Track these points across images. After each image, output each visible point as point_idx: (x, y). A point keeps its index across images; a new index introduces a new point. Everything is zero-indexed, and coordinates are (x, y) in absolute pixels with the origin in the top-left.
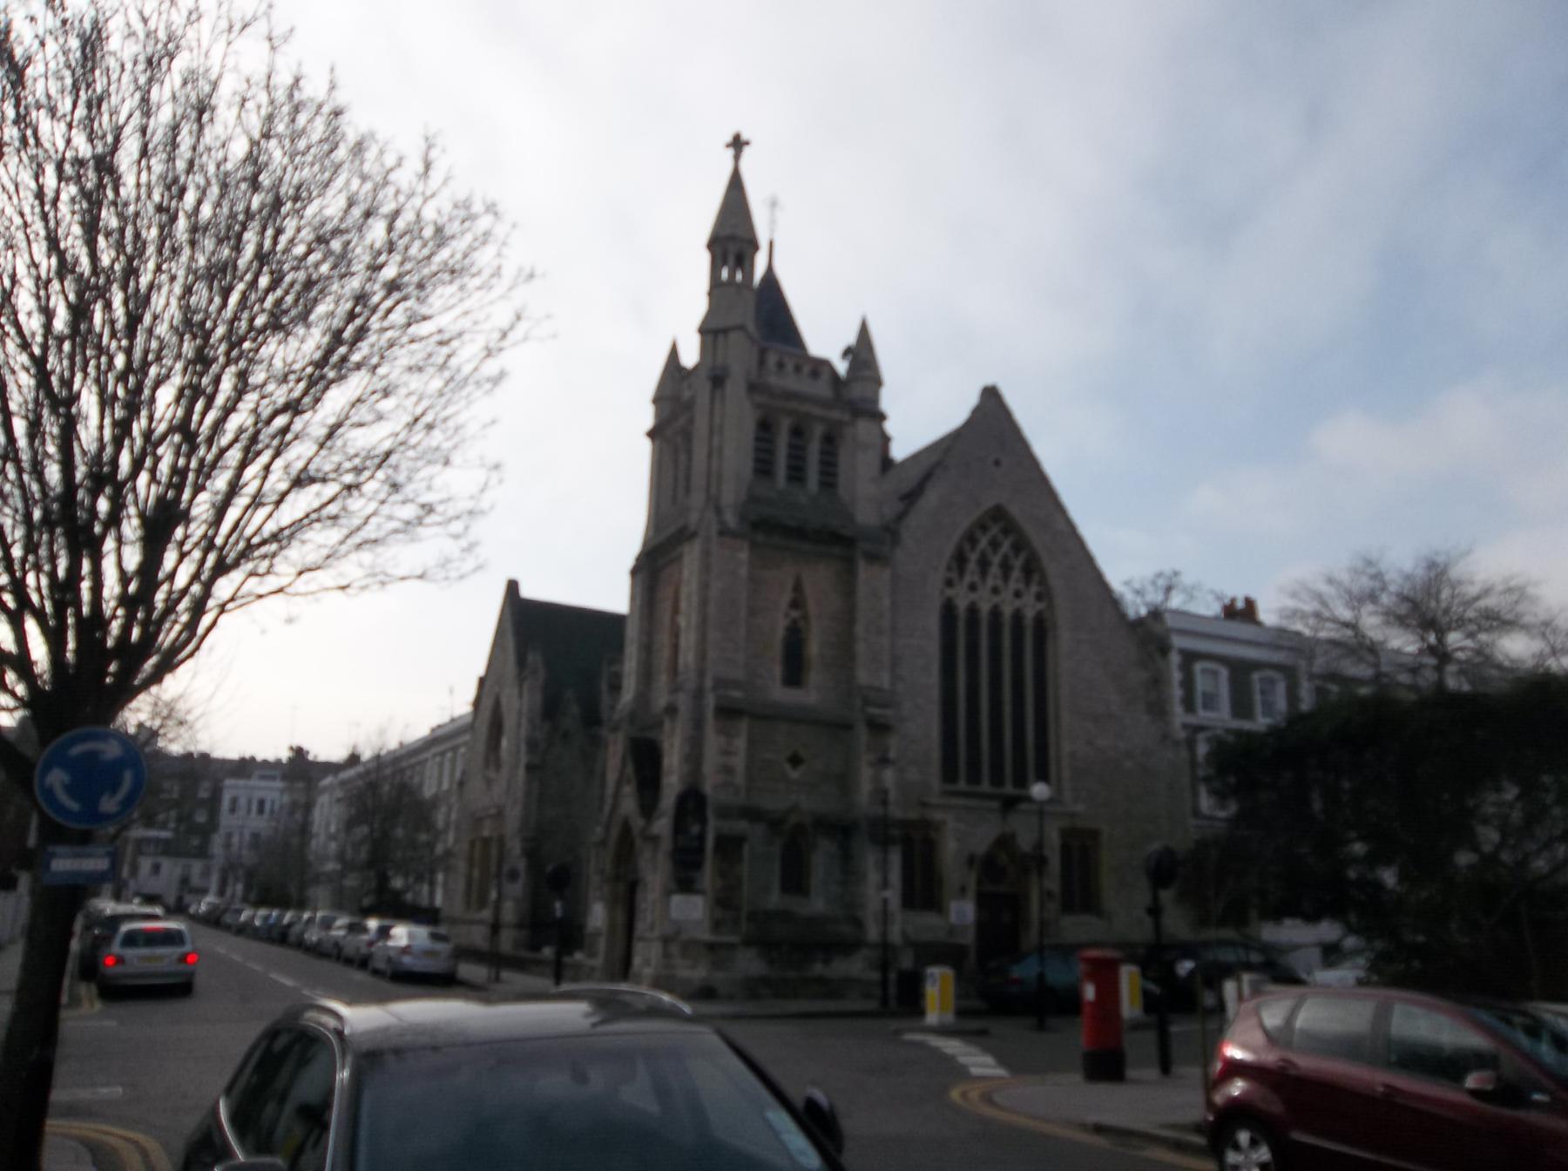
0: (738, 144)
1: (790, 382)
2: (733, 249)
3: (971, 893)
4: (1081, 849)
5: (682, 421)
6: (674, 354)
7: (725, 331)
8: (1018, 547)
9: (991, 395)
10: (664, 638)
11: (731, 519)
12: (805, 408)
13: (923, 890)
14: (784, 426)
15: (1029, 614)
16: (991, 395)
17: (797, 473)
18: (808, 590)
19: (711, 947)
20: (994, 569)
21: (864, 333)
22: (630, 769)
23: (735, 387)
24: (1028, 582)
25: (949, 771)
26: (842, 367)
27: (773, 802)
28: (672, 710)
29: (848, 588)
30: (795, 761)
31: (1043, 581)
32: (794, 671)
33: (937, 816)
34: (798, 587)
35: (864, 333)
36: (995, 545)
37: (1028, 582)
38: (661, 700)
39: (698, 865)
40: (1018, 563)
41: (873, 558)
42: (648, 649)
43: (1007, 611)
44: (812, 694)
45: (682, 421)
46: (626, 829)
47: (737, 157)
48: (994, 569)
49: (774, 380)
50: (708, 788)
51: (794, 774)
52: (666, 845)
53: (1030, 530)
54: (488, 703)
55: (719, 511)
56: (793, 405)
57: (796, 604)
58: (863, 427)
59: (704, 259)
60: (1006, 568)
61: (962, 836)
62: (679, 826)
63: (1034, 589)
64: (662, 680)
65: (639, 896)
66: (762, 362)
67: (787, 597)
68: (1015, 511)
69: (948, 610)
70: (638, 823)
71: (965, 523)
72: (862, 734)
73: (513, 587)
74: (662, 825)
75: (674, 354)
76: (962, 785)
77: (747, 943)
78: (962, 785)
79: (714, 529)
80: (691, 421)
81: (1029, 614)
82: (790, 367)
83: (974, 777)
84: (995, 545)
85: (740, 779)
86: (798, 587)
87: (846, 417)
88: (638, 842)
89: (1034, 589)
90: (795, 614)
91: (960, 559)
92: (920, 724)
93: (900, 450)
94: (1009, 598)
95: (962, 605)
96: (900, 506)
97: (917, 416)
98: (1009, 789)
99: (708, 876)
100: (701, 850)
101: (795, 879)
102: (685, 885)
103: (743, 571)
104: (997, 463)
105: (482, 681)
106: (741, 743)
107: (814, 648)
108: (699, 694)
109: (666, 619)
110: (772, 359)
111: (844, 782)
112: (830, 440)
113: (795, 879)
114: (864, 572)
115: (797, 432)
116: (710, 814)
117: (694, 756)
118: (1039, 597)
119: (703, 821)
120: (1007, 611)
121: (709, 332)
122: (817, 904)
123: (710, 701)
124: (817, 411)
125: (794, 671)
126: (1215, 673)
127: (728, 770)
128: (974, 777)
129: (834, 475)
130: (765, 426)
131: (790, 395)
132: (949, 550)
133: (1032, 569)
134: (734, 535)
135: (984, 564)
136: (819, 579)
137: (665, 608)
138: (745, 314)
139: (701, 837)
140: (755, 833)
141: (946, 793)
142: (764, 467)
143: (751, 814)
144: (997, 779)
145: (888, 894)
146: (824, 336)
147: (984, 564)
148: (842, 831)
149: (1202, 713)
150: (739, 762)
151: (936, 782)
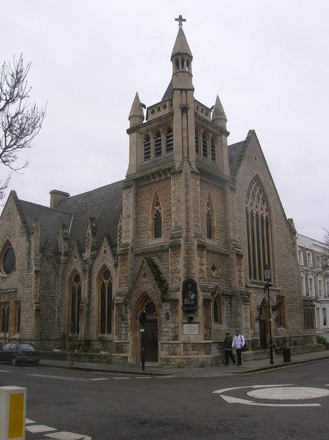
0: (181, 20)
15: (265, 216)
16: (252, 134)
20: (256, 198)
21: (218, 100)
29: (224, 200)
31: (267, 205)
34: (209, 199)
35: (218, 100)
36: (256, 189)
40: (261, 197)
43: (255, 212)
47: (180, 25)
49: (201, 114)
50: (196, 279)
51: (214, 274)
52: (181, 304)
62: (185, 295)
72: (234, 257)
79: (189, 171)
81: (265, 216)
83: (255, 278)
91: (248, 194)
93: (49, 207)
97: (236, 135)
99: (200, 315)
102: (190, 321)
114: (229, 195)
116: (199, 289)
117: (188, 267)
119: (196, 292)
127: (202, 272)
128: (255, 278)
134: (196, 174)
135: (254, 196)
139: (196, 299)
141: (252, 283)
147: (254, 196)
148: (230, 297)
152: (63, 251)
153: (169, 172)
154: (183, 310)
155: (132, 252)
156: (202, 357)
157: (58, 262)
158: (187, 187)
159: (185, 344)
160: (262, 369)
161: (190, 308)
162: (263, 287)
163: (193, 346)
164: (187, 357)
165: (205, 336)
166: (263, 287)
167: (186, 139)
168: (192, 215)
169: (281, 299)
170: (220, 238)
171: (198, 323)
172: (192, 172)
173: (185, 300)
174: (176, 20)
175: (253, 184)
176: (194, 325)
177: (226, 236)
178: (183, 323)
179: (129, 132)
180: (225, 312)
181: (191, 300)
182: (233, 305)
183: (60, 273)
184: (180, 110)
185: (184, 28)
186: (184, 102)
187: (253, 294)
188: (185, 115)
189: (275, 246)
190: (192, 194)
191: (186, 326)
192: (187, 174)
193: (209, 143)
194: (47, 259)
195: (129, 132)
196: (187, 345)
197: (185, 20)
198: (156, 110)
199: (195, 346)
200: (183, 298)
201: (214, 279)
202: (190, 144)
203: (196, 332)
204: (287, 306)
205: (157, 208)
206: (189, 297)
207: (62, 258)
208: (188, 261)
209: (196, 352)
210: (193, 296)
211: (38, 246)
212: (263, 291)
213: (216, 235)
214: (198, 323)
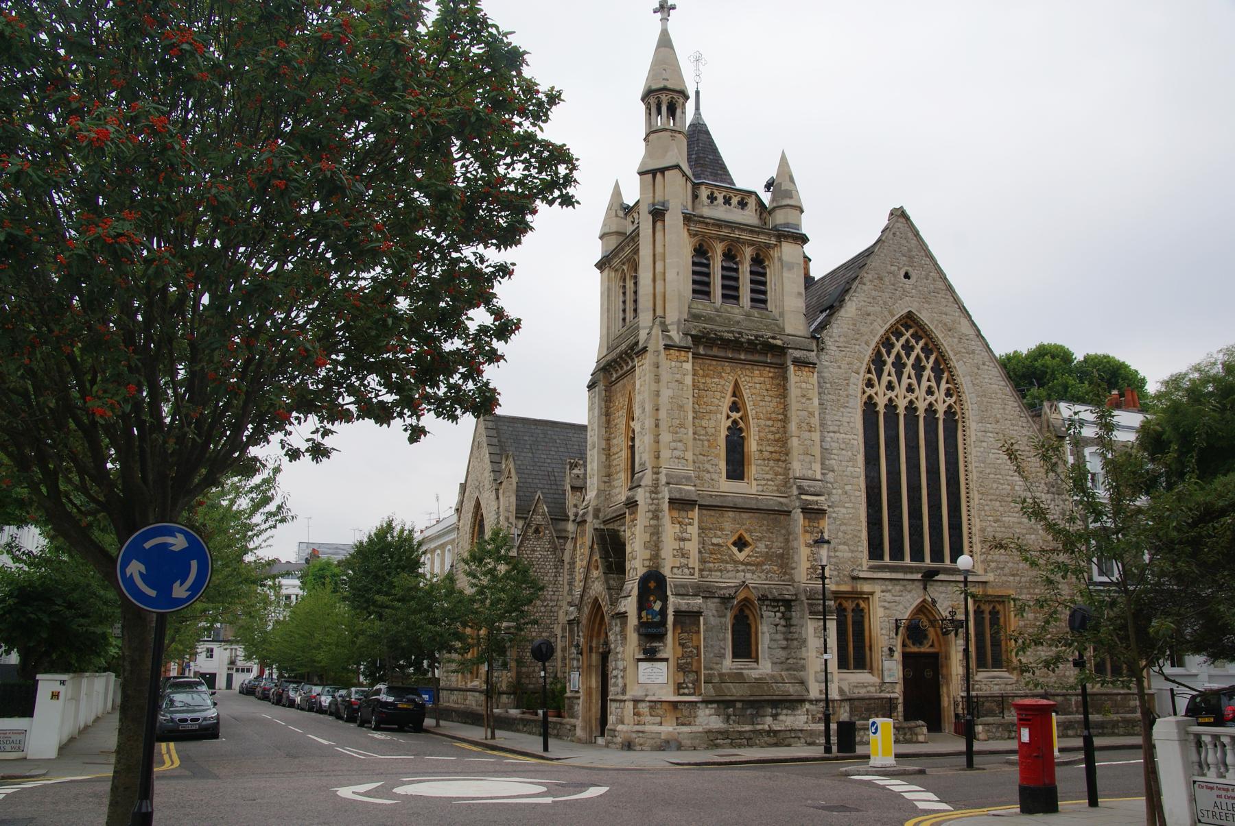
0: (664, 8)
8: (927, 350)
9: (899, 215)
15: (941, 409)
21: (784, 161)
32: (736, 469)
33: (866, 588)
34: (736, 392)
35: (784, 161)
36: (908, 348)
47: (665, 20)
49: (707, 211)
50: (666, 572)
51: (741, 556)
52: (633, 620)
53: (939, 334)
57: (735, 407)
62: (643, 604)
68: (924, 316)
69: (870, 405)
84: (908, 348)
89: (944, 386)
97: (832, 239)
99: (669, 648)
102: (650, 655)
117: (655, 546)
118: (948, 394)
119: (664, 599)
124: (745, 236)
135: (899, 366)
139: (663, 612)
147: (899, 366)
148: (785, 605)
154: (640, 634)
155: (596, 516)
156: (668, 729)
158: (657, 379)
159: (636, 702)
160: (689, 764)
161: (654, 631)
162: (919, 576)
163: (651, 708)
166: (919, 576)
167: (658, 277)
168: (666, 437)
170: (769, 477)
171: (666, 660)
173: (644, 614)
175: (899, 335)
178: (639, 660)
179: (601, 265)
180: (767, 635)
181: (654, 614)
182: (794, 621)
185: (671, 27)
186: (659, 198)
187: (878, 595)
188: (659, 224)
189: (974, 476)
191: (642, 665)
194: (537, 531)
195: (601, 265)
201: (741, 567)
202: (641, 291)
203: (663, 679)
206: (650, 607)
207: (571, 527)
210: (657, 606)
211: (513, 508)
212: (921, 586)
213: (753, 470)
214: (666, 660)
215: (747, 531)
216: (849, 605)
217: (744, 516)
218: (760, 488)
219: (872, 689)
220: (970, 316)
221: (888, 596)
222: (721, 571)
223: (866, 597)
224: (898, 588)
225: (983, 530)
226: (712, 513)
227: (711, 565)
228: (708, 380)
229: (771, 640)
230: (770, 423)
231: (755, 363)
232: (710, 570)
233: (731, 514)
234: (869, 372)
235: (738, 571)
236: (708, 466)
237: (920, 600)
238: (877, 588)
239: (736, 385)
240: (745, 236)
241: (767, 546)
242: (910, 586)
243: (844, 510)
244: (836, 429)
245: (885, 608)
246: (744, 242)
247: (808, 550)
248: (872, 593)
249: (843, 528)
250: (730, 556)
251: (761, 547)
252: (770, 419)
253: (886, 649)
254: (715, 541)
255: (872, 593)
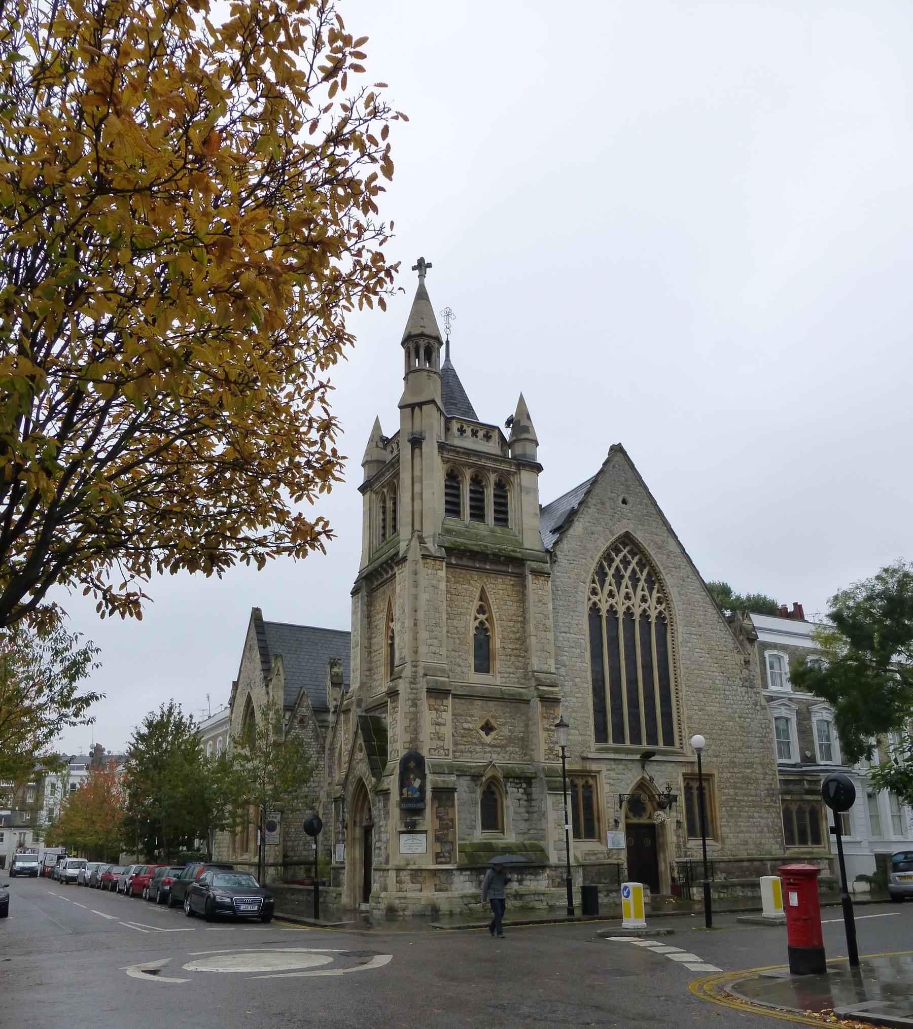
1: (469, 443)
2: (423, 343)
3: (622, 826)
4: (699, 784)
5: (388, 475)
6: (377, 426)
7: (420, 405)
10: (380, 641)
11: (432, 548)
12: (482, 462)
13: (586, 824)
14: (467, 475)
15: (653, 614)
16: (617, 451)
17: (478, 513)
18: (491, 598)
19: (434, 873)
22: (361, 741)
23: (430, 447)
24: (651, 590)
25: (601, 735)
26: (507, 433)
27: (476, 760)
28: (393, 693)
29: (522, 598)
30: (488, 728)
31: (661, 590)
32: (483, 662)
33: (594, 767)
34: (483, 597)
36: (625, 562)
37: (651, 590)
38: (382, 686)
39: (419, 812)
41: (537, 573)
42: (369, 649)
44: (500, 678)
45: (388, 475)
46: (361, 784)
47: (422, 276)
48: (626, 581)
49: (457, 442)
50: (425, 753)
51: (488, 739)
52: (395, 797)
53: (651, 551)
54: (241, 701)
55: (421, 540)
56: (472, 460)
57: (481, 610)
58: (525, 476)
59: (400, 353)
60: (635, 580)
61: (614, 784)
62: (404, 782)
63: (655, 595)
64: (382, 671)
65: (374, 837)
66: (447, 429)
67: (476, 604)
68: (639, 536)
69: (595, 610)
70: (370, 782)
71: (603, 545)
73: (256, 614)
74: (392, 783)
75: (377, 426)
76: (611, 743)
77: (461, 869)
78: (611, 743)
80: (397, 475)
81: (653, 614)
82: (469, 433)
84: (625, 562)
85: (448, 744)
86: (483, 597)
87: (513, 469)
88: (371, 796)
89: (655, 595)
90: (482, 617)
91: (601, 573)
92: (578, 702)
94: (637, 601)
95: (604, 607)
96: (556, 537)
97: (562, 471)
98: (645, 746)
99: (428, 821)
100: (422, 799)
101: (491, 819)
102: (411, 829)
103: (443, 586)
104: (624, 502)
105: (235, 685)
106: (448, 716)
107: (497, 643)
108: (414, 681)
109: (382, 626)
110: (455, 426)
111: (525, 743)
112: (501, 488)
113: (491, 819)
115: (477, 481)
117: (414, 730)
118: (659, 601)
119: (423, 777)
120: (637, 612)
121: (409, 407)
122: (510, 838)
123: (423, 685)
124: (490, 464)
125: (483, 662)
126: (779, 658)
129: (506, 513)
130: (452, 478)
131: (469, 452)
132: (594, 566)
133: (654, 579)
135: (618, 577)
136: (499, 590)
137: (380, 619)
138: (434, 390)
140: (463, 786)
141: (600, 750)
142: (453, 508)
143: (461, 772)
144: (636, 739)
145: (567, 827)
146: (492, 409)
147: (618, 577)
148: (526, 780)
149: (772, 688)
150: (447, 731)
151: (593, 745)
152: (331, 706)
153: (397, 560)
154: (402, 810)
157: (324, 725)
158: (416, 584)
161: (413, 806)
163: (411, 875)
164: (401, 894)
165: (437, 855)
166: (638, 757)
168: (424, 635)
169: (699, 784)
171: (425, 832)
172: (425, 557)
174: (414, 268)
175: (618, 551)
176: (419, 836)
177: (526, 665)
182: (534, 796)
183: (327, 746)
184: (409, 445)
187: (604, 773)
188: (417, 451)
190: (424, 597)
191: (404, 837)
192: (415, 561)
193: (490, 493)
195: (363, 489)
196: (588, 869)
197: (429, 265)
198: (481, 434)
199: (417, 874)
200: (402, 785)
201: (488, 749)
203: (422, 849)
204: (720, 796)
205: (595, 598)
206: (410, 785)
208: (414, 718)
209: (418, 886)
210: (417, 783)
212: (639, 765)
213: (498, 664)
214: (425, 832)
215: (493, 717)
216: (580, 782)
217: (491, 704)
218: (504, 680)
219: (601, 856)
220: (676, 537)
221: (613, 774)
222: (471, 752)
223: (594, 775)
224: (621, 767)
225: (690, 718)
226: (463, 701)
227: (463, 747)
228: (459, 586)
229: (516, 813)
230: (511, 624)
231: (498, 572)
232: (462, 752)
233: (479, 702)
234: (594, 582)
235: (485, 753)
236: (459, 661)
237: (639, 778)
238: (603, 767)
239: (483, 591)
240: (490, 464)
241: (510, 731)
242: (630, 765)
243: (574, 700)
244: (567, 629)
245: (611, 785)
246: (489, 469)
247: (545, 734)
248: (599, 772)
249: (575, 714)
250: (478, 739)
251: (505, 732)
252: (511, 621)
253: (612, 821)
254: (466, 726)
255: (599, 772)
